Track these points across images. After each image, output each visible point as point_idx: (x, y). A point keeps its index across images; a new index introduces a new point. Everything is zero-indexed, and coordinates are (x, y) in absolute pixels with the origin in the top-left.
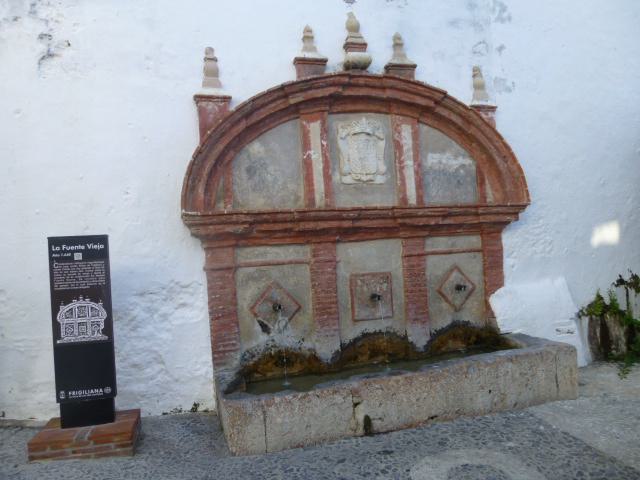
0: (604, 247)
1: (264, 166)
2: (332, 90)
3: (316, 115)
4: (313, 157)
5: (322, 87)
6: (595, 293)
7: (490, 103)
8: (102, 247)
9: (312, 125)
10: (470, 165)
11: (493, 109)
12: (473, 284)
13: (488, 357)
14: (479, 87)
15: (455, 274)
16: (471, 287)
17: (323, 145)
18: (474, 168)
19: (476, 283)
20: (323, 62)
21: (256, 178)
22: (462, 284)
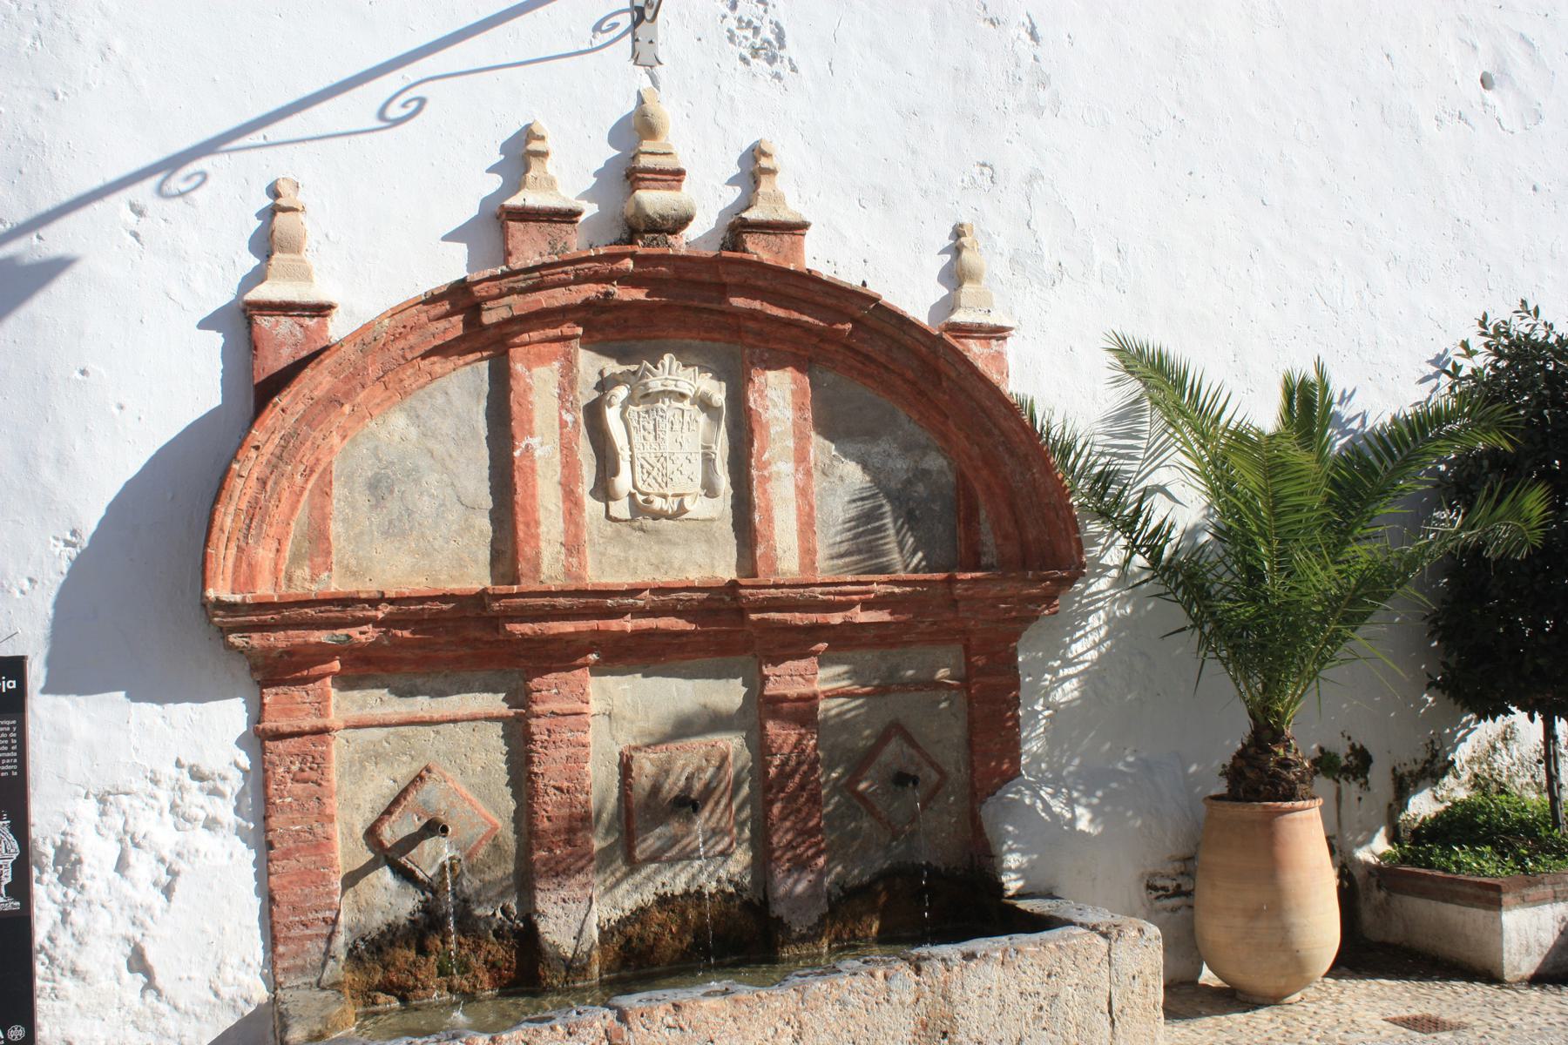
0: (1435, 647)
1: (413, 475)
2: (591, 291)
3: (546, 349)
4: (538, 453)
5: (564, 284)
6: (172, 904)
7: (993, 320)
8: (12, 684)
9: (538, 371)
10: (941, 472)
11: (998, 333)
12: (941, 772)
13: (835, 975)
14: (956, 275)
15: (894, 747)
16: (935, 777)
17: (563, 424)
18: (951, 478)
19: (950, 768)
20: (321, 310)
21: (393, 505)
22: (912, 770)
